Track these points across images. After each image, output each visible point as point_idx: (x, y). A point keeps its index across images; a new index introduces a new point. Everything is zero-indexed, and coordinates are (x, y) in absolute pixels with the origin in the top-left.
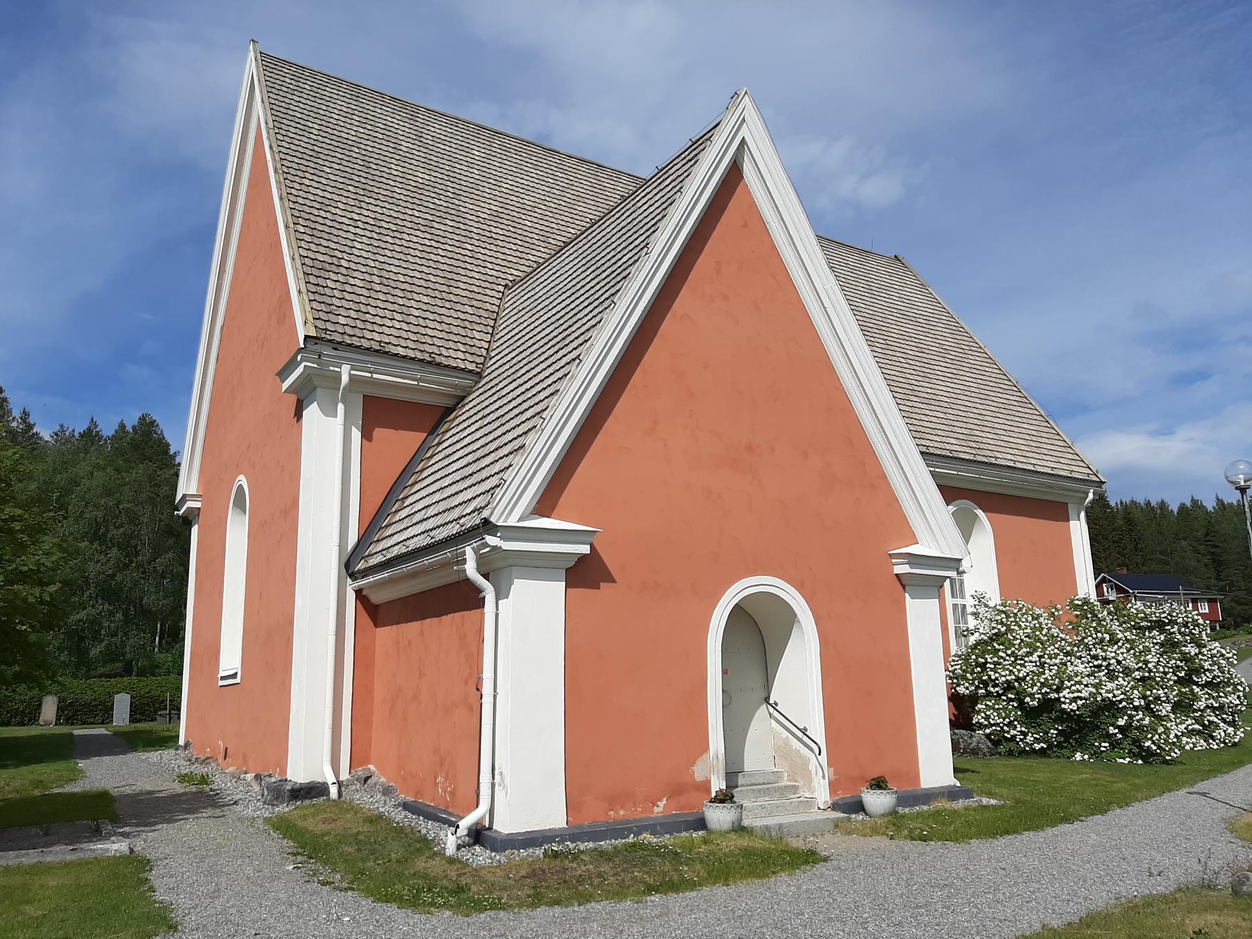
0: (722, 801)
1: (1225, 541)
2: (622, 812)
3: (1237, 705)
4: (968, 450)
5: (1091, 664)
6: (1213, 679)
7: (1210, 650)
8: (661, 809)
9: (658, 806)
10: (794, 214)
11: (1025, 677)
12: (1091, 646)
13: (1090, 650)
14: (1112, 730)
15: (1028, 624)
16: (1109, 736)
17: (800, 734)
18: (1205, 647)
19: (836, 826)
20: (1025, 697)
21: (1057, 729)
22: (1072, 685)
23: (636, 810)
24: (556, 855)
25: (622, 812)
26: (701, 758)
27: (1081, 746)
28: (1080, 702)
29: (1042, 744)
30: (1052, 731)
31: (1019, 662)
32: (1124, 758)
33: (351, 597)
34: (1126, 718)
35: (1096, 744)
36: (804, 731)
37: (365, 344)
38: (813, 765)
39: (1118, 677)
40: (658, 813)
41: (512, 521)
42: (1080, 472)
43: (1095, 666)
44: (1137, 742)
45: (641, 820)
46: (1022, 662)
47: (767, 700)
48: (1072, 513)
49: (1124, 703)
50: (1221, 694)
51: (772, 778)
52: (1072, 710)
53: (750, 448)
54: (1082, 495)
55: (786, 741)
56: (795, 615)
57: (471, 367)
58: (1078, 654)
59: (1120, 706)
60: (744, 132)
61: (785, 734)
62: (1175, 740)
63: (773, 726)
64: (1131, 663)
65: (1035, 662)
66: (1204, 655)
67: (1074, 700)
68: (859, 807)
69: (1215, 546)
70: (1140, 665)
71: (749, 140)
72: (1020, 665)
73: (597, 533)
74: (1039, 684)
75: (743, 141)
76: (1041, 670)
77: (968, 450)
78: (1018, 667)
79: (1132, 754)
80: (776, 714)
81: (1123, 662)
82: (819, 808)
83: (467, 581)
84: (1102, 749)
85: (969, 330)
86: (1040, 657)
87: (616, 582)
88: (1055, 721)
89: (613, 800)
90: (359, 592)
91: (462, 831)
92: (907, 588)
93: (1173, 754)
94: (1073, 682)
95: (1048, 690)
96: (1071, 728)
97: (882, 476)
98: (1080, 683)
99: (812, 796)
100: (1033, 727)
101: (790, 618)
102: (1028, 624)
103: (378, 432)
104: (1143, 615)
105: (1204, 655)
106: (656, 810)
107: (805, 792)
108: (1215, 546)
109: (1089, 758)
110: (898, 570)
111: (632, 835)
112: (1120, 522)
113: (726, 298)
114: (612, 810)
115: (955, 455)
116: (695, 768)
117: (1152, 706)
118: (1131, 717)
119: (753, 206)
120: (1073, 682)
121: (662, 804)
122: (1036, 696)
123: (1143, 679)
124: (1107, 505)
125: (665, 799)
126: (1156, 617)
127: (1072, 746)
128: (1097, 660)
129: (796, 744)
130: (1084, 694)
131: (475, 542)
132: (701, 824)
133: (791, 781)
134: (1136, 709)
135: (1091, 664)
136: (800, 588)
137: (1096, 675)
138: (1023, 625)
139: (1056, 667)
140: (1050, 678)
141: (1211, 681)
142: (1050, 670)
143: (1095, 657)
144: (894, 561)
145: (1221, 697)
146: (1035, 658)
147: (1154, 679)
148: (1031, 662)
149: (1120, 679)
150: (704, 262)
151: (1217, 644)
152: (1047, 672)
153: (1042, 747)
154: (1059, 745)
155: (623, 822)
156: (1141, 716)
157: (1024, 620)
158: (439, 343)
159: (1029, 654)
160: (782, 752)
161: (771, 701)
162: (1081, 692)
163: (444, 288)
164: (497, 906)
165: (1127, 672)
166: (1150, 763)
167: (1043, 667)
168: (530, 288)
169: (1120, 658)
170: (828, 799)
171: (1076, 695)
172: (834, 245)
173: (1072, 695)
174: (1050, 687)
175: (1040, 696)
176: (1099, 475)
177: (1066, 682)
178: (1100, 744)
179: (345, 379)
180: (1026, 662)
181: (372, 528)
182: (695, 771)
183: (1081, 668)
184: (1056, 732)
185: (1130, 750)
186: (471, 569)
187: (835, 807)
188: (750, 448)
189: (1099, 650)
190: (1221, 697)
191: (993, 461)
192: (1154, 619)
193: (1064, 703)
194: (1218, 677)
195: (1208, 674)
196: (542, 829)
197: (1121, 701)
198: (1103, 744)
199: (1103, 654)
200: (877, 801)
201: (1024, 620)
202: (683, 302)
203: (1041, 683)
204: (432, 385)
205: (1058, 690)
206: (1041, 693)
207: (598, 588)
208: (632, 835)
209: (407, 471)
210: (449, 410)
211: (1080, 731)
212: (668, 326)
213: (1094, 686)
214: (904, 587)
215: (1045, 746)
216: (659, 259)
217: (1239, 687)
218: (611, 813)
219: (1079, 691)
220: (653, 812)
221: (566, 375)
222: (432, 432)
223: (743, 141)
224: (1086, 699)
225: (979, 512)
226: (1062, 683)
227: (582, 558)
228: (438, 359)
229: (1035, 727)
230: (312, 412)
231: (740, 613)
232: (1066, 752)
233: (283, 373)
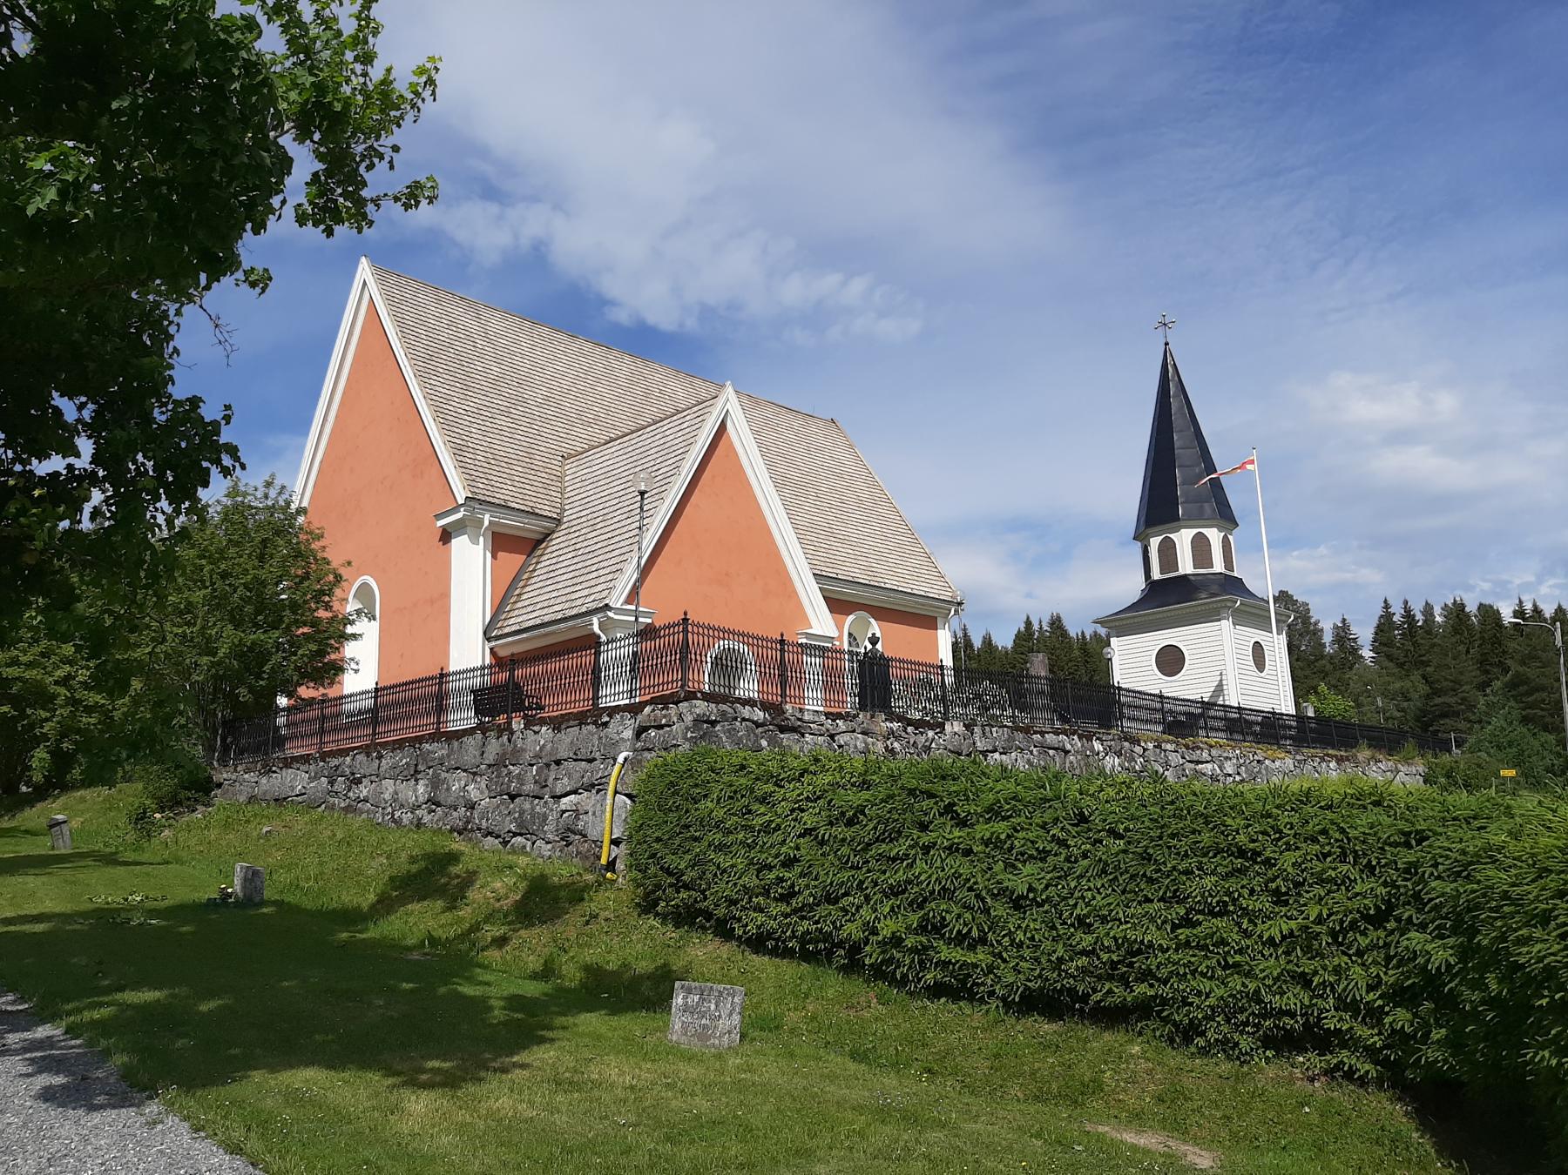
4: (866, 577)
33: (488, 651)
37: (497, 501)
41: (618, 606)
42: (946, 595)
48: (939, 625)
57: (555, 516)
60: (728, 405)
71: (730, 410)
77: (866, 577)
83: (594, 633)
85: (881, 484)
90: (491, 649)
97: (795, 592)
101: (744, 662)
103: (500, 554)
112: (1077, 653)
115: (856, 580)
124: (1065, 634)
158: (534, 500)
163: (528, 460)
172: (783, 410)
179: (486, 523)
181: (501, 606)
188: (727, 575)
191: (882, 585)
204: (533, 527)
209: (516, 579)
210: (540, 542)
222: (528, 556)
225: (872, 620)
228: (537, 511)
230: (460, 544)
231: (717, 661)
233: (439, 517)
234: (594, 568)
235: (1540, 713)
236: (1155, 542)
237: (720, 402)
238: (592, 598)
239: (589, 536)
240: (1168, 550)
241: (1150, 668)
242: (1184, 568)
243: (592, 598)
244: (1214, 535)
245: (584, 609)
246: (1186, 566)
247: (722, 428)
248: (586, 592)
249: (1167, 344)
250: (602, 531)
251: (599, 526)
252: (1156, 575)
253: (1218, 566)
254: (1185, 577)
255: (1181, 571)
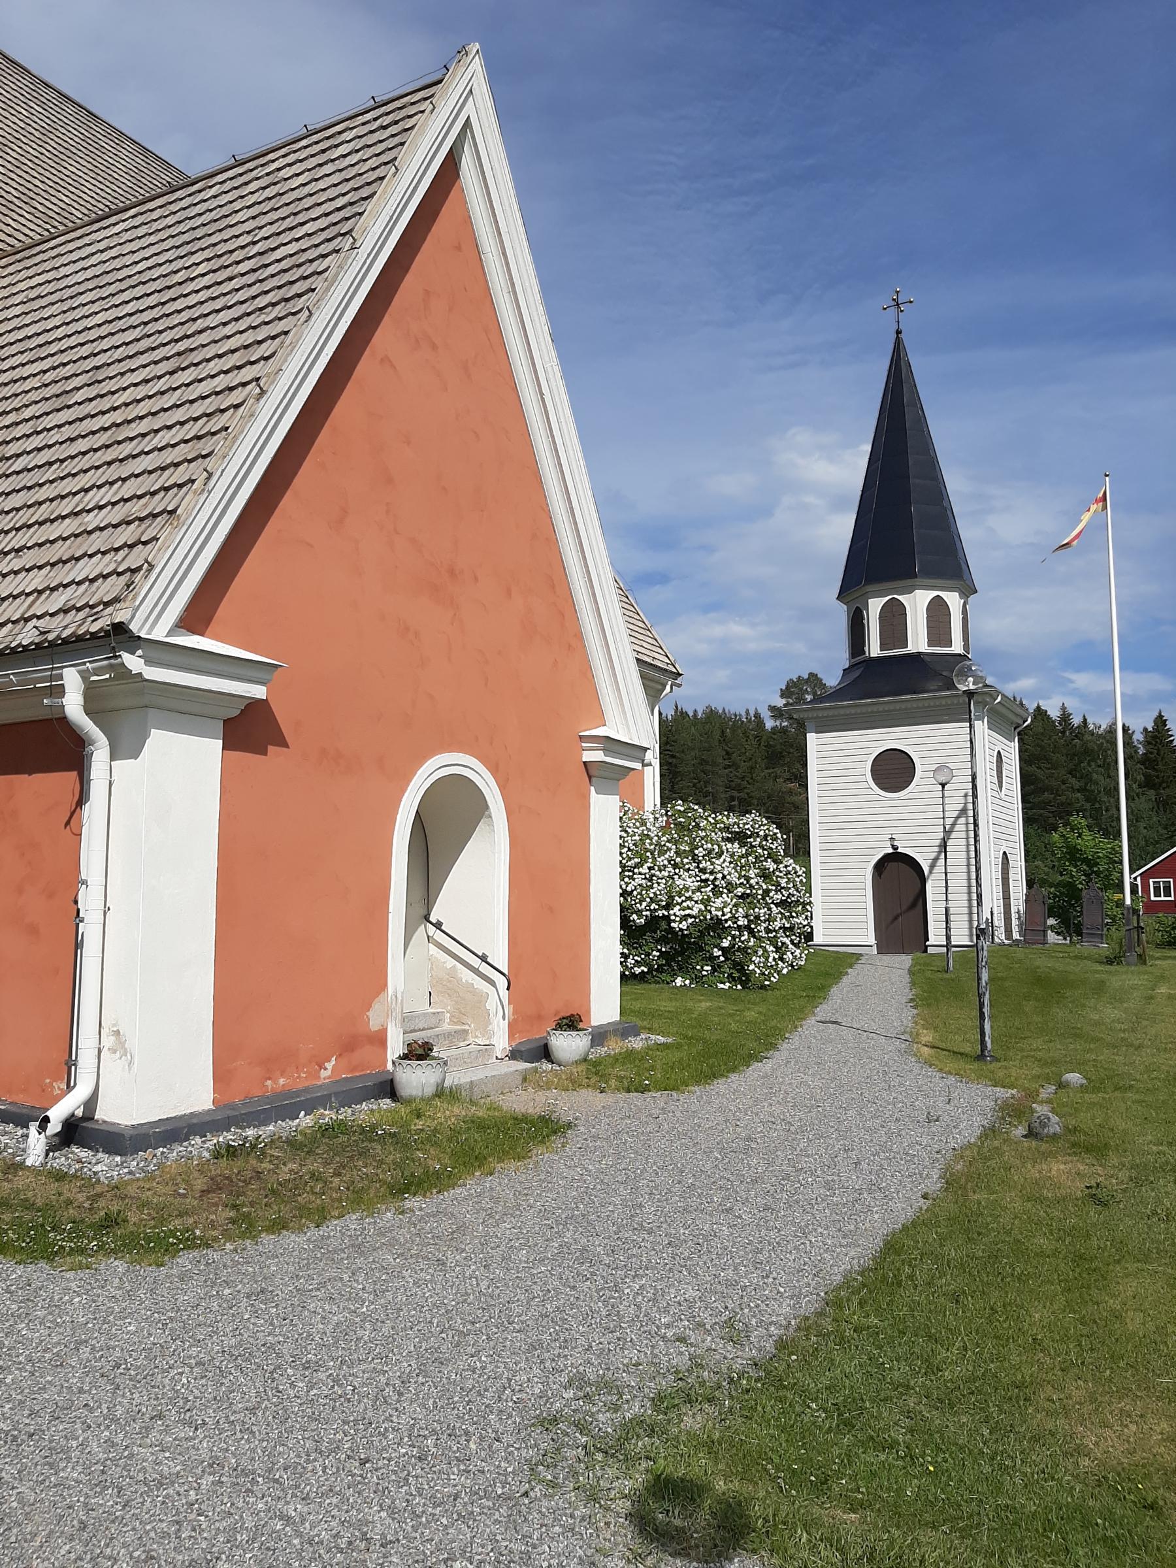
0: (420, 1058)
1: (683, 752)
2: (282, 1081)
3: (804, 926)
5: (698, 879)
6: (788, 897)
7: (786, 867)
8: (329, 1073)
9: (326, 1069)
10: (518, 249)
11: (632, 891)
12: (701, 858)
13: (700, 862)
14: (717, 952)
15: (636, 830)
16: (712, 958)
17: (475, 962)
18: (781, 863)
19: (525, 1080)
20: (632, 913)
21: (659, 951)
22: (683, 901)
23: (299, 1077)
24: (231, 1151)
25: (282, 1081)
26: (377, 1000)
27: (683, 970)
28: (690, 921)
29: (643, 968)
30: (654, 953)
31: (627, 873)
32: (724, 983)
34: (729, 938)
35: (698, 967)
36: (484, 959)
38: (492, 1004)
39: (722, 893)
40: (324, 1079)
41: (159, 633)
43: (702, 881)
44: (740, 967)
45: (306, 1090)
46: (631, 874)
47: (427, 918)
49: (730, 923)
50: (794, 914)
51: (433, 1021)
52: (681, 930)
53: (452, 572)
54: (660, 687)
55: (453, 971)
56: (487, 807)
58: (687, 867)
59: (726, 925)
60: (469, 110)
61: (451, 962)
62: (773, 963)
63: (431, 953)
64: (734, 878)
65: (645, 874)
66: (781, 872)
67: (685, 917)
68: (545, 1052)
69: (673, 756)
70: (742, 880)
72: (628, 876)
73: (280, 669)
74: (648, 900)
75: (467, 123)
76: (649, 884)
78: (626, 880)
79: (731, 978)
80: (439, 936)
81: (728, 877)
82: (497, 1058)
84: (704, 973)
86: (650, 868)
87: (287, 746)
88: (658, 941)
89: (272, 1063)
91: (54, 1127)
92: (594, 779)
93: (772, 979)
94: (683, 898)
95: (657, 907)
96: (675, 949)
97: (579, 636)
98: (690, 899)
99: (488, 1043)
100: (634, 948)
101: (480, 808)
102: (636, 830)
104: (722, 825)
105: (781, 872)
106: (323, 1074)
107: (476, 1037)
108: (673, 756)
109: (691, 983)
110: (588, 756)
111: (303, 1113)
113: (434, 347)
114: (269, 1079)
116: (370, 1014)
117: (753, 926)
118: (734, 937)
119: (468, 221)
120: (683, 898)
121: (329, 1066)
122: (644, 913)
123: (743, 896)
125: (334, 1059)
126: (739, 827)
127: (673, 970)
128: (705, 873)
129: (466, 975)
130: (695, 912)
131: (90, 662)
132: (389, 1089)
133: (455, 1023)
134: (739, 928)
135: (698, 879)
136: (494, 770)
137: (703, 890)
138: (629, 830)
139: (664, 881)
140: (658, 893)
141: (786, 900)
142: (659, 884)
143: (703, 871)
144: (584, 745)
145: (793, 917)
146: (644, 870)
147: (755, 896)
148: (640, 874)
149: (724, 896)
150: (411, 283)
151: (792, 861)
152: (655, 885)
153: (643, 971)
154: (660, 969)
155: (289, 1094)
156: (746, 937)
157: (631, 825)
159: (638, 865)
160: (442, 987)
161: (433, 919)
162: (692, 909)
164: (190, 1242)
165: (730, 887)
166: (749, 988)
167: (650, 880)
168: (47, 266)
169: (726, 873)
170: (507, 1045)
171: (687, 912)
173: (683, 913)
174: (657, 903)
175: (648, 913)
176: (677, 666)
177: (677, 898)
178: (702, 967)
180: (634, 874)
182: (371, 1016)
183: (689, 882)
184: (658, 954)
185: (730, 975)
186: (73, 705)
187: (514, 1055)
189: (708, 863)
190: (793, 917)
192: (737, 830)
193: (674, 921)
194: (793, 895)
195: (784, 893)
196: (180, 1114)
197: (726, 921)
198: (706, 968)
199: (712, 867)
200: (568, 1045)
201: (631, 825)
202: (384, 337)
203: (651, 898)
205: (668, 907)
206: (650, 910)
207: (266, 754)
208: (303, 1113)
211: (682, 953)
212: (366, 367)
213: (702, 901)
214: (590, 777)
215: (646, 970)
216: (368, 262)
217: (808, 907)
218: (269, 1083)
219: (689, 908)
220: (319, 1077)
221: (237, 407)
223: (467, 123)
224: (694, 917)
226: (672, 898)
227: (255, 707)
229: (636, 948)
232: (664, 976)
234: (66, 507)
235: (1046, 814)
236: (875, 605)
237: (447, 100)
238: (59, 600)
239: (48, 422)
240: (894, 618)
241: (862, 778)
242: (916, 642)
243: (59, 600)
244: (953, 600)
245: (27, 636)
246: (918, 641)
247: (449, 171)
248: (37, 580)
249: (898, 332)
250: (90, 408)
251: (79, 396)
252: (874, 649)
253: (957, 647)
254: (919, 655)
255: (911, 648)
